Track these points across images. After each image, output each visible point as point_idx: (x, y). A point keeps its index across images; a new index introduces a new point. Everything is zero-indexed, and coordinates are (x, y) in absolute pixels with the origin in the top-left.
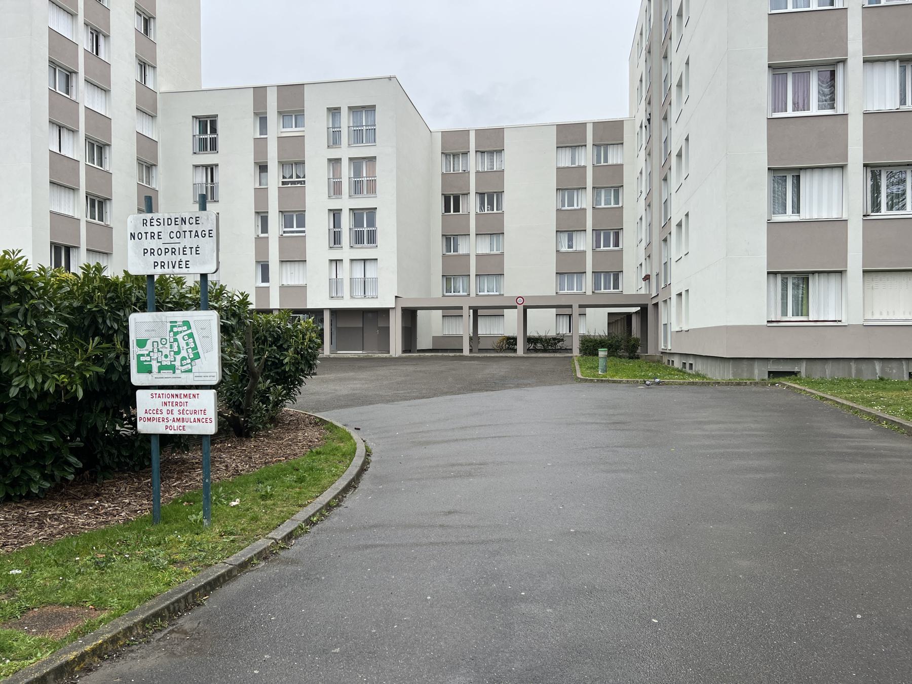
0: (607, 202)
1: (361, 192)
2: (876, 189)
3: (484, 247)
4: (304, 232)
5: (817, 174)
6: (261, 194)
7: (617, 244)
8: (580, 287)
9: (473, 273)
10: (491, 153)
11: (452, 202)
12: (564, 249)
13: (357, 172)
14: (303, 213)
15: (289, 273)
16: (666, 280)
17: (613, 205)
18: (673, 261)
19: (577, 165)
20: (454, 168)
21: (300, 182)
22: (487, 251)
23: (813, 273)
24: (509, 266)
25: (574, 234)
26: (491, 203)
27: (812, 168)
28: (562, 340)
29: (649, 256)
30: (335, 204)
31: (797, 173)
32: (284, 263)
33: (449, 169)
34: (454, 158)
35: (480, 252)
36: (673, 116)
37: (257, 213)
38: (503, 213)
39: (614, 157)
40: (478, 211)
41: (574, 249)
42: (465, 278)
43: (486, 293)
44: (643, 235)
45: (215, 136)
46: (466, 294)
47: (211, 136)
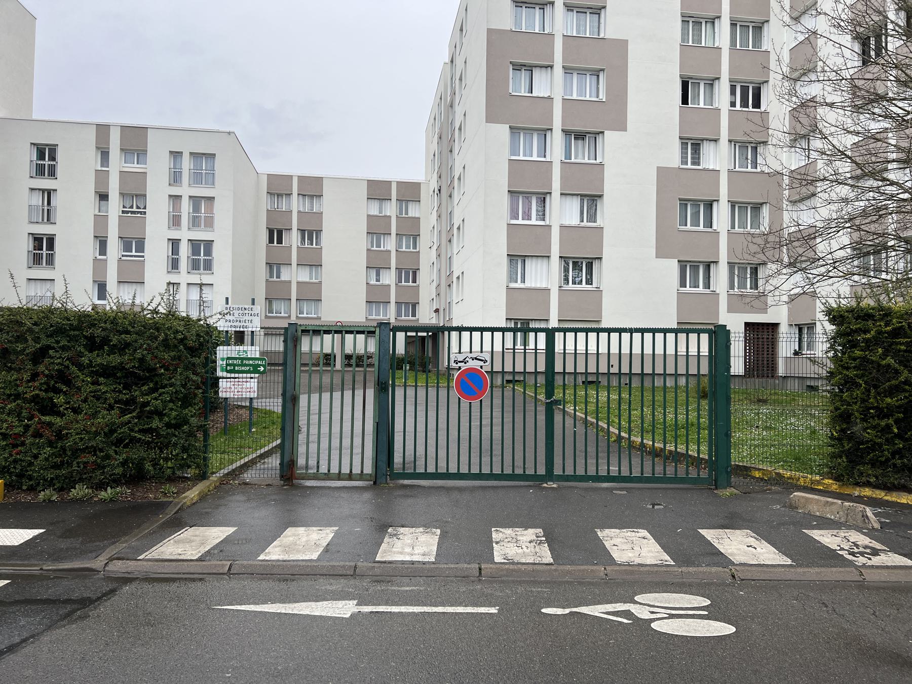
0: (408, 247)
1: (199, 226)
2: (566, 270)
3: (304, 275)
4: (143, 256)
5: (534, 259)
6: (101, 221)
7: (414, 281)
8: (385, 314)
9: (294, 297)
10: (312, 197)
11: (276, 235)
12: (373, 282)
13: (196, 209)
14: (143, 240)
15: (126, 293)
16: (449, 316)
17: (412, 250)
18: (455, 302)
19: (383, 214)
20: (278, 206)
21: (141, 213)
22: (307, 279)
23: (532, 320)
24: (326, 293)
25: (381, 271)
26: (310, 238)
27: (532, 256)
28: (371, 357)
29: (439, 294)
30: (175, 235)
31: (524, 258)
32: (121, 283)
33: (273, 206)
34: (278, 198)
35: (300, 280)
36: (456, 151)
37: (95, 237)
38: (321, 248)
39: (413, 211)
40: (299, 245)
41: (381, 282)
42: (287, 302)
43: (305, 315)
44: (435, 277)
45: (54, 163)
46: (287, 315)
47: (49, 163)
